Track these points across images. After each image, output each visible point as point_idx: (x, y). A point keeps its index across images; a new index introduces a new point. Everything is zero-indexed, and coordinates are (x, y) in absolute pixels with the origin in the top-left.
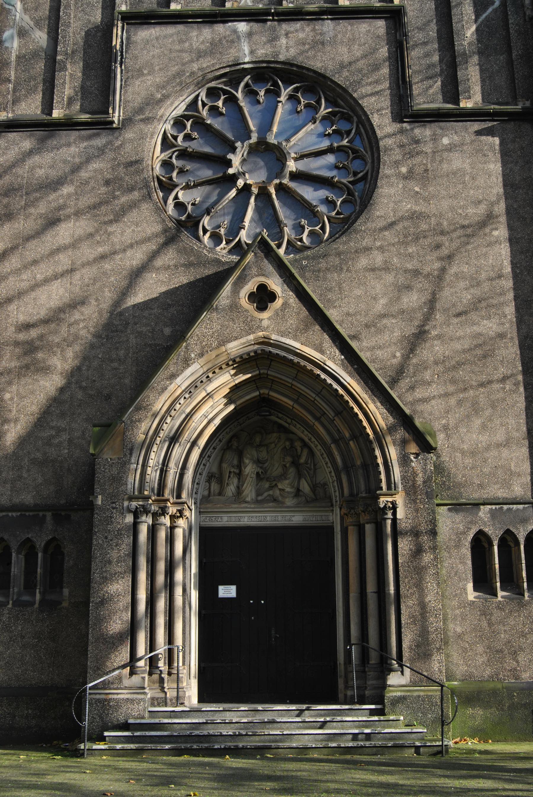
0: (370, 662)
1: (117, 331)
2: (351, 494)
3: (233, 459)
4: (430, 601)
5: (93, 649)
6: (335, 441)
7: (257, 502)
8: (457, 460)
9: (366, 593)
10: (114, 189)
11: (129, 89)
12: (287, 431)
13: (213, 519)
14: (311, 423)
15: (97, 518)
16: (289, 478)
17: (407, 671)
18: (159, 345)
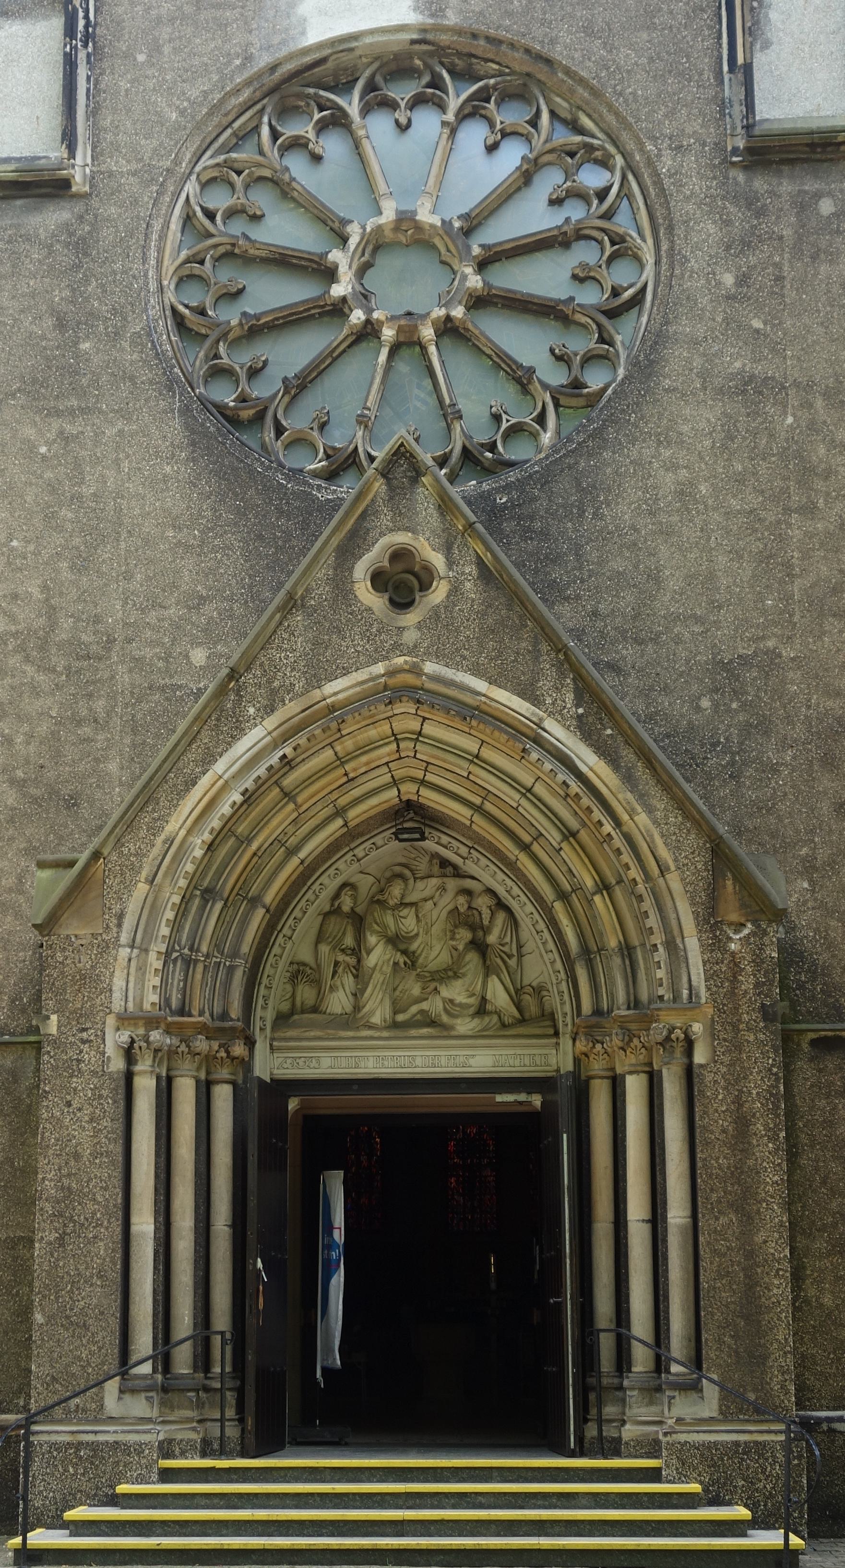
0: (634, 1369)
1: (90, 658)
2: (597, 1012)
3: (344, 934)
4: (765, 1242)
5: (43, 1339)
6: (563, 896)
7: (395, 1025)
8: (833, 935)
9: (626, 1222)
10: (76, 337)
11: (105, 100)
12: (458, 873)
13: (301, 1061)
14: (509, 855)
15: (48, 1062)
16: (464, 975)
18: (180, 687)
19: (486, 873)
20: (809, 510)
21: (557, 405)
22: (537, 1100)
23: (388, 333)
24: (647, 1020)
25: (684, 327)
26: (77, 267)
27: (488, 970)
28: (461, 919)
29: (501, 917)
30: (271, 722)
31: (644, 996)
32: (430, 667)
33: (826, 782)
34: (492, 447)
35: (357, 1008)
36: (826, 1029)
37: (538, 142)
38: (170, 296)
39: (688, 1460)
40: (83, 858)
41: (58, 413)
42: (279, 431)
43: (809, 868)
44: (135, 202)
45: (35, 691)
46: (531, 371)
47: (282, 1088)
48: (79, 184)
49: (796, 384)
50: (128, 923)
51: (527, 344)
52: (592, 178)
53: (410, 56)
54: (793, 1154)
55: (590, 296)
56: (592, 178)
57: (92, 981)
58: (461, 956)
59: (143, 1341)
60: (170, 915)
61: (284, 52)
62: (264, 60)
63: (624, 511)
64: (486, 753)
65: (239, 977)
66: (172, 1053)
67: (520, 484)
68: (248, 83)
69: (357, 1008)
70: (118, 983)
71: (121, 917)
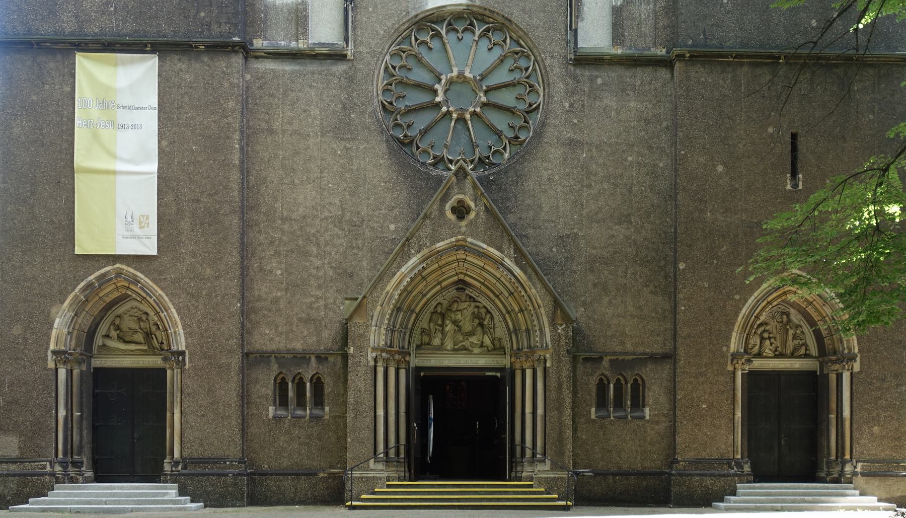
2: (518, 349)
6: (508, 312)
7: (454, 350)
12: (475, 301)
17: (548, 462)
19: (485, 302)
20: (589, 186)
21: (510, 143)
22: (498, 375)
23: (455, 116)
24: (533, 353)
25: (551, 121)
26: (349, 86)
27: (484, 333)
28: (476, 316)
29: (488, 315)
30: (419, 256)
31: (532, 345)
32: (469, 240)
33: (591, 277)
34: (488, 158)
35: (442, 344)
36: (587, 355)
37: (506, 48)
38: (381, 98)
39: (540, 482)
40: (360, 297)
41: (344, 140)
42: (418, 148)
43: (584, 304)
44: (369, 64)
45: (338, 237)
46: (502, 132)
47: (418, 369)
48: (349, 56)
49: (587, 143)
50: (375, 319)
51: (500, 121)
52: (523, 63)
53: (463, 13)
54: (575, 393)
55: (522, 106)
56: (523, 63)
57: (364, 337)
58: (476, 328)
59: (381, 447)
60: (388, 316)
61: (420, 11)
62: (413, 13)
63: (531, 184)
64: (486, 267)
65: (407, 335)
66: (388, 359)
67: (497, 173)
68: (408, 21)
69: (442, 344)
70: (372, 338)
71: (372, 317)
